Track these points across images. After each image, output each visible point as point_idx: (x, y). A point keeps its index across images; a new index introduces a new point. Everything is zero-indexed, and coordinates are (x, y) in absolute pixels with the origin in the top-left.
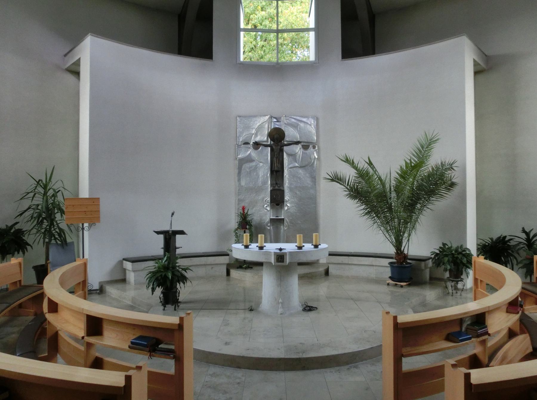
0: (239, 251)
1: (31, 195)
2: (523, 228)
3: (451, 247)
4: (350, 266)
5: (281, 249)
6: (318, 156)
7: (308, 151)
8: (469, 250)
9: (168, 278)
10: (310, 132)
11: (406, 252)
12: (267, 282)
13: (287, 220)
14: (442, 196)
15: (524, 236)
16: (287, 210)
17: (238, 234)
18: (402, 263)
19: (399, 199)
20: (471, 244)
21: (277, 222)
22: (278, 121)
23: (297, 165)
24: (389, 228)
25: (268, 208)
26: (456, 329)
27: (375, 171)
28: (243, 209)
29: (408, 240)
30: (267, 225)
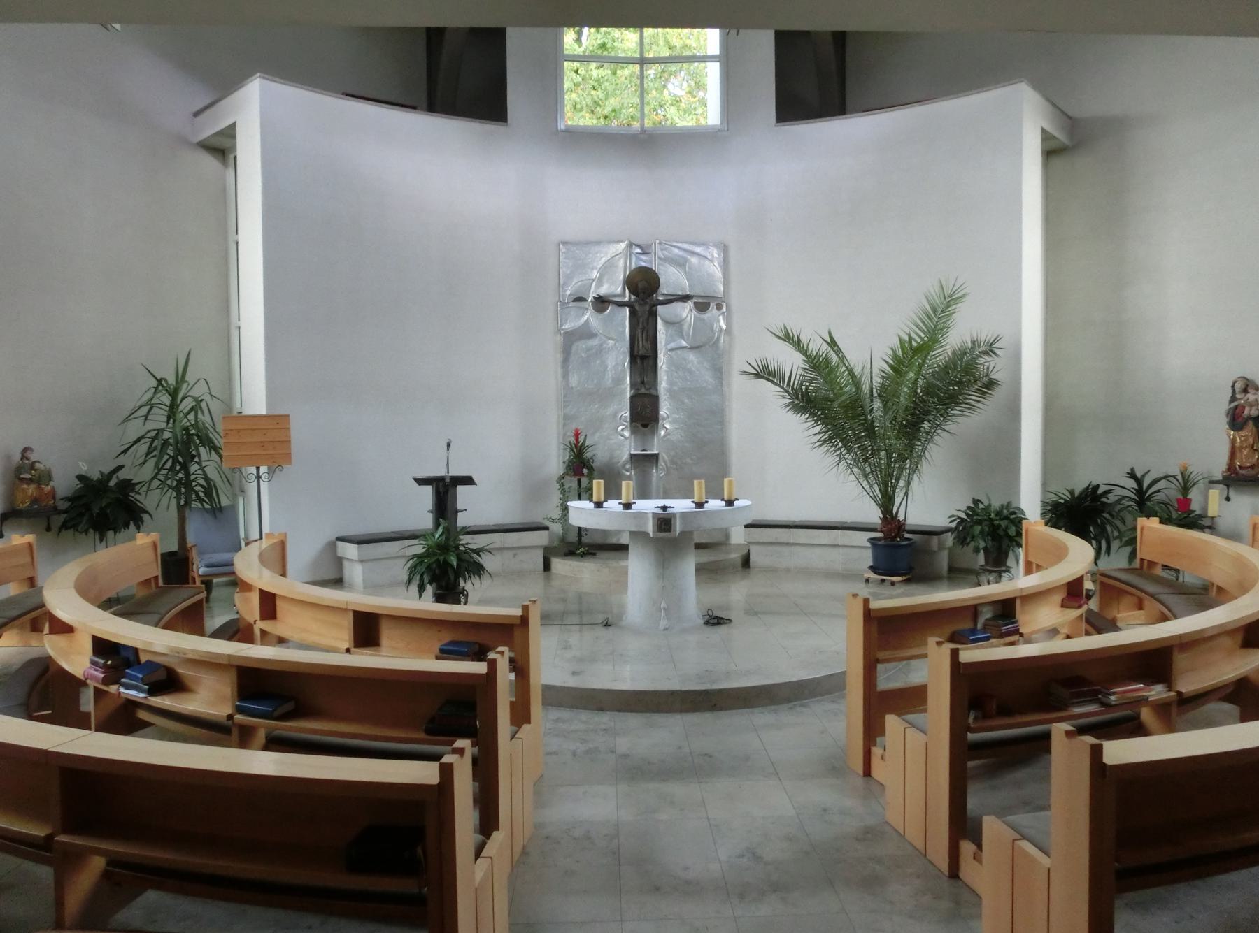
0: (582, 513)
1: (145, 410)
2: (1132, 470)
3: (990, 505)
4: (793, 549)
5: (664, 508)
6: (727, 325)
7: (706, 316)
8: (1022, 512)
9: (452, 566)
10: (710, 275)
11: (901, 517)
12: (638, 569)
13: (664, 457)
14: (971, 407)
15: (1131, 484)
17: (566, 487)
18: (893, 539)
19: (888, 411)
20: (1030, 503)
21: (644, 461)
22: (644, 253)
23: (684, 343)
24: (868, 470)
25: (627, 434)
26: (967, 625)
27: (842, 358)
28: (577, 435)
29: (906, 493)
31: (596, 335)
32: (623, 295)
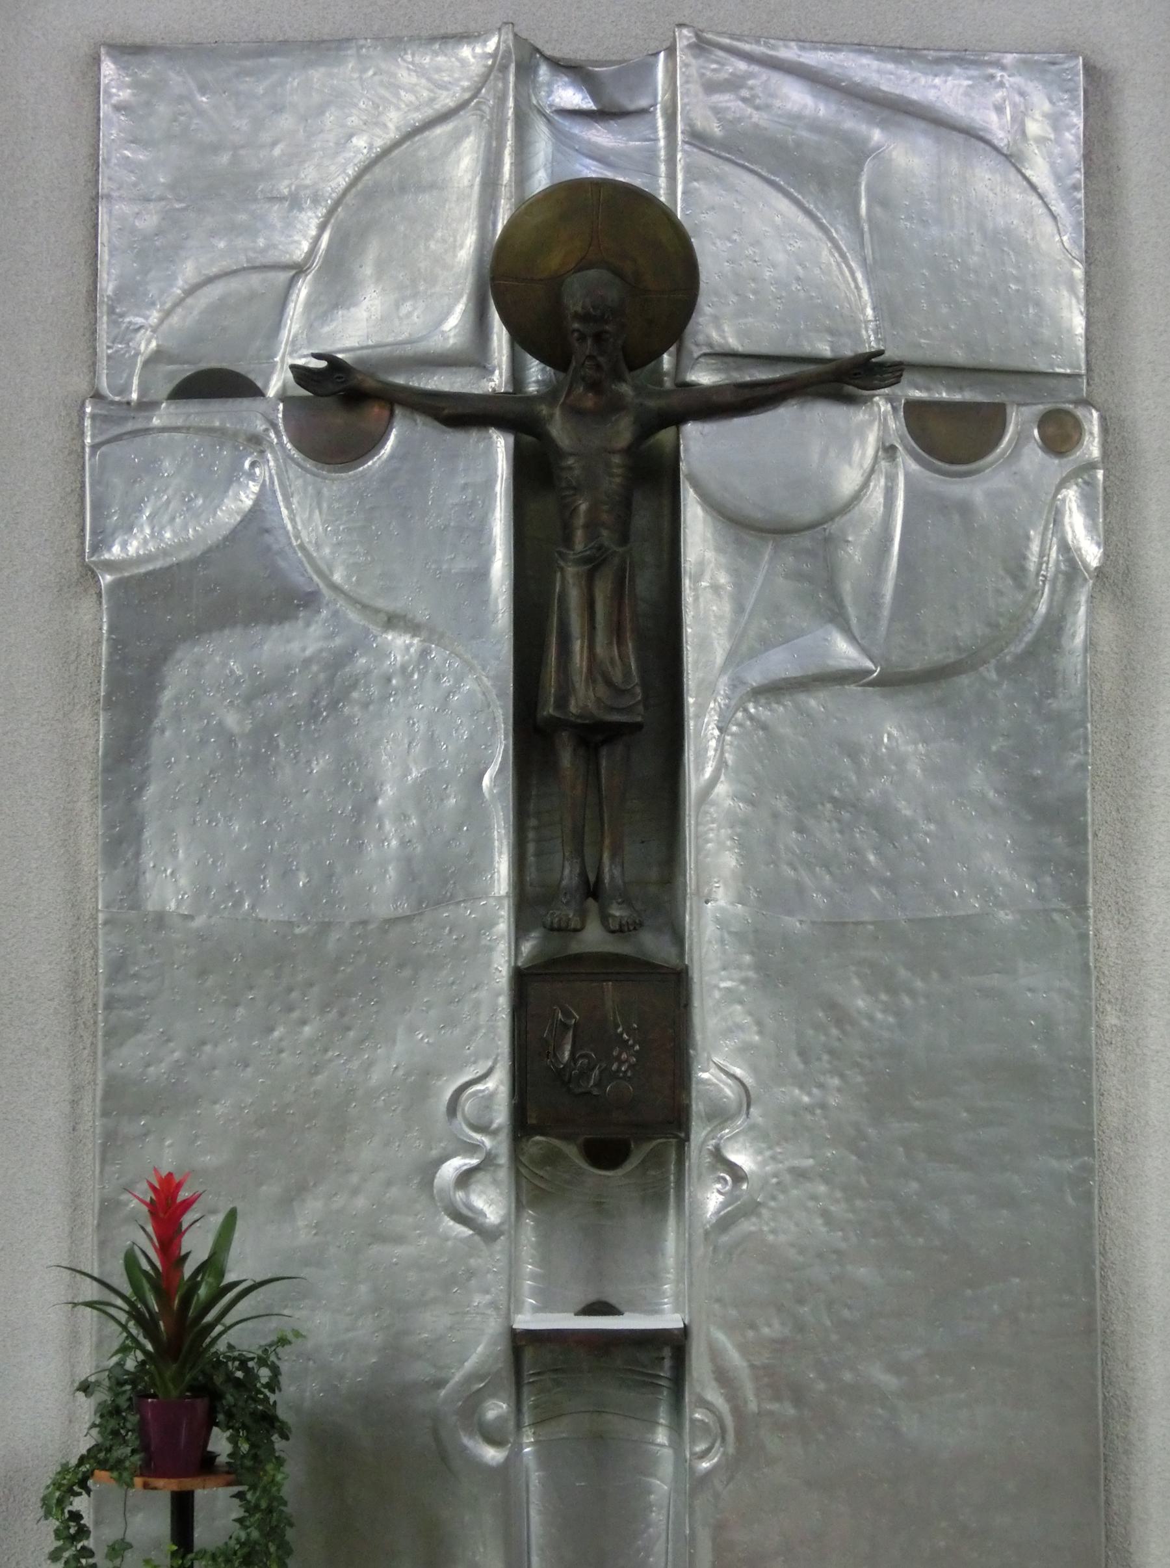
6: (1107, 542)
7: (980, 488)
13: (719, 1348)
16: (725, 1222)
22: (604, 114)
23: (844, 651)
25: (489, 1204)
28: (168, 1208)
30: (471, 1405)
31: (308, 601)
32: (475, 357)
